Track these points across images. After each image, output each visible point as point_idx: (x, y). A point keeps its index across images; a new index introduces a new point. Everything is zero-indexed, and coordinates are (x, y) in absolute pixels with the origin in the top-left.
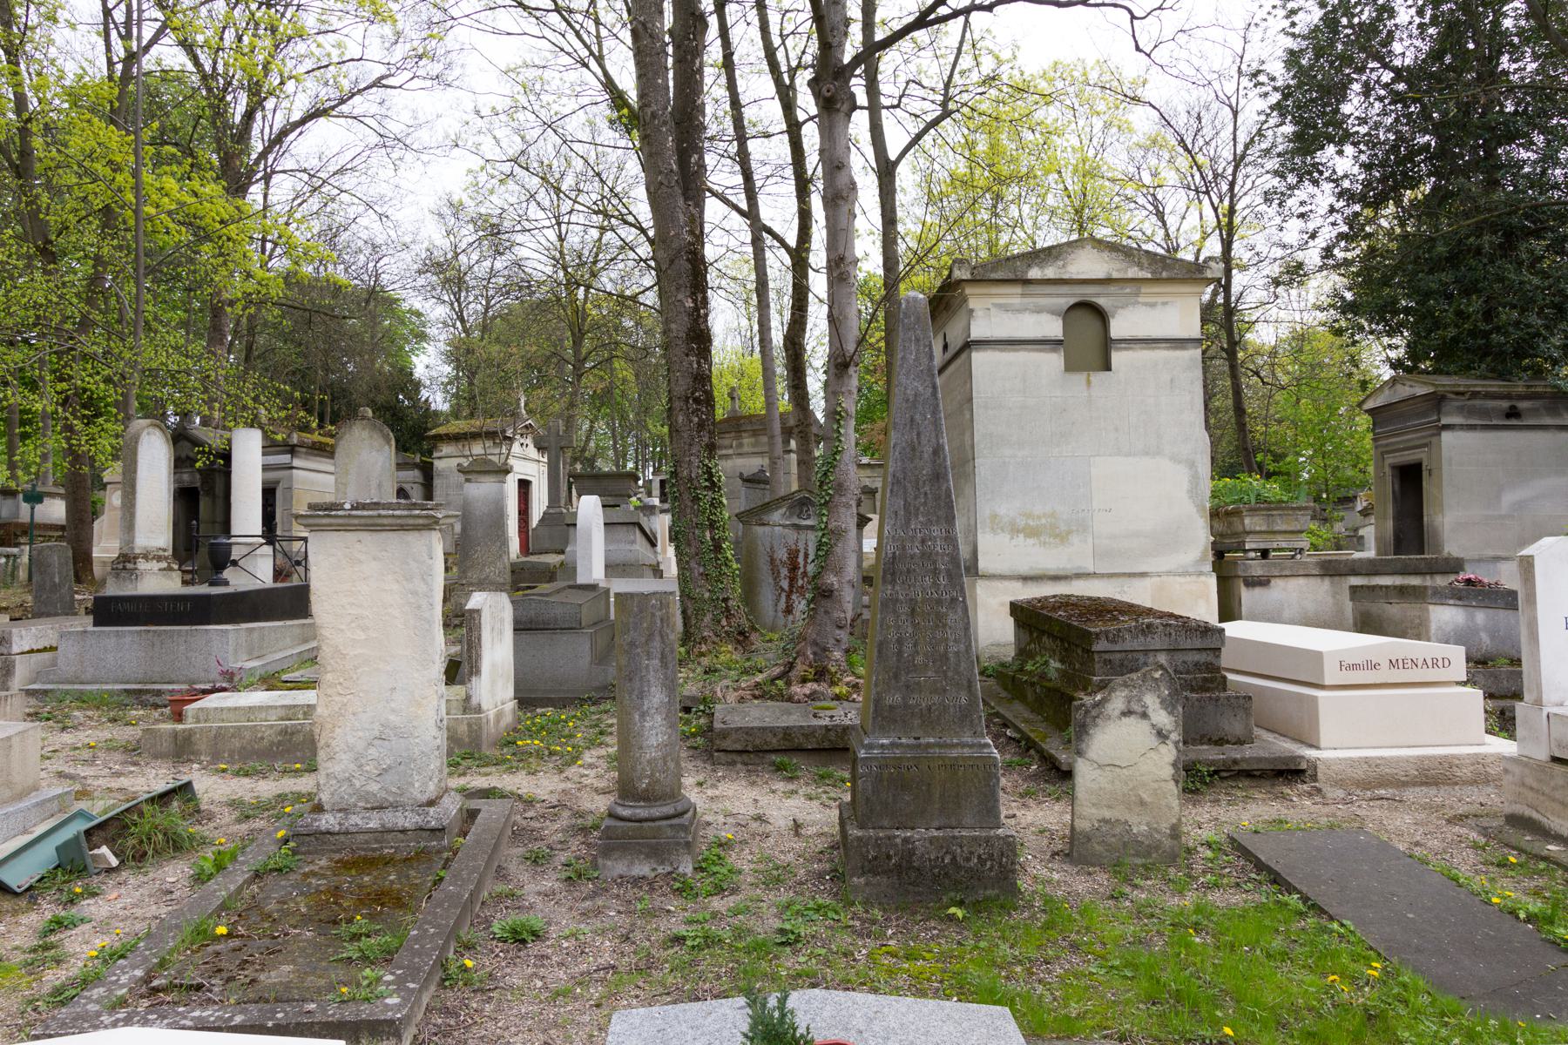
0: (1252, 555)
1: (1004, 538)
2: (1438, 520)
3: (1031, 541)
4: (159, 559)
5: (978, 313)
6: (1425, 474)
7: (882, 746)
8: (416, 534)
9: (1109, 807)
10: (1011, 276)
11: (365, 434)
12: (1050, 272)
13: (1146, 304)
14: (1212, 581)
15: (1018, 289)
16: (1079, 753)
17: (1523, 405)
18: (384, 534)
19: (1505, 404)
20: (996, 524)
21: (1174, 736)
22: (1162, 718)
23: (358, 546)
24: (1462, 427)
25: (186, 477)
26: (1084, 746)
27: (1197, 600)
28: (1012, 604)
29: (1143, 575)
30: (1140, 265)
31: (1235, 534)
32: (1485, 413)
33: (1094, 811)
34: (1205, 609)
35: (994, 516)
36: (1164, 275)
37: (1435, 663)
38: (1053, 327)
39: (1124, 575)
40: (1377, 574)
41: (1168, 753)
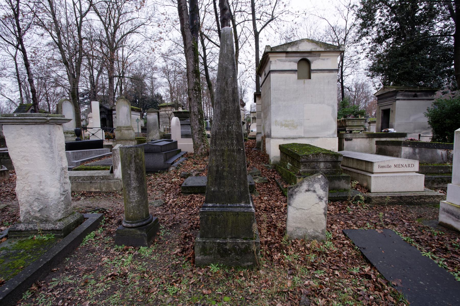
0: (348, 132)
1: (279, 127)
2: (393, 123)
3: (286, 128)
4: (71, 133)
5: (273, 62)
6: (391, 112)
7: (209, 207)
8: (43, 126)
9: (300, 223)
10: (282, 50)
11: (123, 102)
12: (294, 49)
13: (322, 59)
14: (337, 139)
15: (284, 55)
16: (289, 204)
17: (418, 94)
18: (31, 126)
19: (413, 93)
20: (276, 123)
21: (325, 199)
22: (321, 193)
23: (22, 130)
24: (402, 99)
25: (103, 116)
26: (291, 202)
27: (331, 144)
28: (280, 146)
29: (318, 138)
30: (321, 47)
31: (343, 127)
32: (408, 96)
33: (294, 224)
34: (336, 150)
35: (276, 121)
36: (328, 50)
37: (409, 166)
38: (294, 66)
39: (314, 138)
40: (398, 137)
41: (323, 205)
